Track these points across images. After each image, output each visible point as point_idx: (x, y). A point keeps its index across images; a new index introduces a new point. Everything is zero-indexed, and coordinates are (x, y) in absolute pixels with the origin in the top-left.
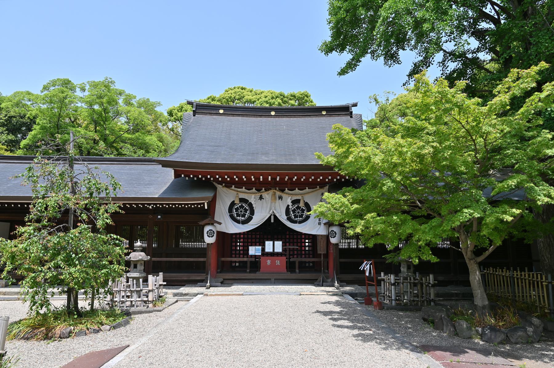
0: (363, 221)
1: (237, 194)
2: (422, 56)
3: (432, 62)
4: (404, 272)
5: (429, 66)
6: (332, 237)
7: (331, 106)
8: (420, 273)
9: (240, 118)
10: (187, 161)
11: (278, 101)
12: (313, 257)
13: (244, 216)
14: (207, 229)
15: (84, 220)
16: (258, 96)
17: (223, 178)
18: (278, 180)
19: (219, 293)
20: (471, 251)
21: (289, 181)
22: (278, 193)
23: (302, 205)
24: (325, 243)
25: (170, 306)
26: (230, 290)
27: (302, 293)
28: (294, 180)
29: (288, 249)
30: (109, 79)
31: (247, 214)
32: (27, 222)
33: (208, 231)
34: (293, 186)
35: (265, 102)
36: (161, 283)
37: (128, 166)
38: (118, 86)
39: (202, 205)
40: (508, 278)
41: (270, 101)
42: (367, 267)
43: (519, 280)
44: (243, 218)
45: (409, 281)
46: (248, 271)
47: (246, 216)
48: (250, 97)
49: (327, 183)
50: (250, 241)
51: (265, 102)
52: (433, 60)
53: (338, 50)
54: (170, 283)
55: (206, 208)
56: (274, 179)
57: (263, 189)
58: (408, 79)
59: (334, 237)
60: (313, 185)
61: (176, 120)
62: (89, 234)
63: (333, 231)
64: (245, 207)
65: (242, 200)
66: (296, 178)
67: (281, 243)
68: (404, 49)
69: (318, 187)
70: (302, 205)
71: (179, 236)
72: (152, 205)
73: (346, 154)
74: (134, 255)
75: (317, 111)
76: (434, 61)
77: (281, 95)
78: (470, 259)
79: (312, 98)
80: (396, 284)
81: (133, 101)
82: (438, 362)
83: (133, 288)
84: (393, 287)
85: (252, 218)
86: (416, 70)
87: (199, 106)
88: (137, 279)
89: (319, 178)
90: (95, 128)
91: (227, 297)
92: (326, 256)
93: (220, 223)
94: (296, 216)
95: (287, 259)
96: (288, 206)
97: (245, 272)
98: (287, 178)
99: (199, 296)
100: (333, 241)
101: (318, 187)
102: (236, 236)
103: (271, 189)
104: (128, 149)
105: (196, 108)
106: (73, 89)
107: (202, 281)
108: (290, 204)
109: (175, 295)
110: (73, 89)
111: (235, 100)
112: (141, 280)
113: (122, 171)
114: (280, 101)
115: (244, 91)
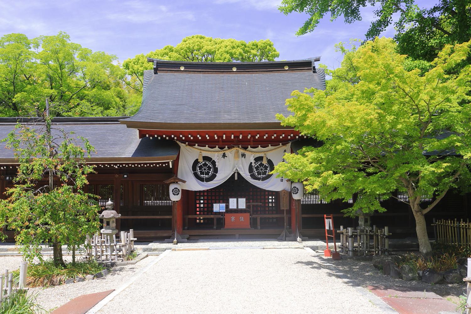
0: (321, 178)
1: (201, 152)
2: (380, 16)
3: (390, 22)
4: (361, 225)
5: (387, 25)
6: (294, 194)
7: (294, 61)
8: (377, 227)
9: (201, 75)
10: (151, 121)
11: (239, 50)
12: (277, 214)
13: (207, 173)
14: (172, 187)
15: (65, 181)
16: (218, 46)
17: (187, 137)
18: (241, 138)
19: (186, 248)
20: (418, 204)
21: (252, 139)
22: (241, 151)
23: (265, 162)
24: (288, 198)
25: (142, 259)
26: (196, 245)
27: (265, 247)
28: (257, 138)
29: (252, 206)
30: (63, 33)
31: (211, 172)
32: (15, 184)
33: (173, 190)
34: (255, 143)
35: (225, 52)
36: (132, 239)
37: (92, 126)
38: (73, 41)
39: (167, 164)
40: (456, 228)
41: (231, 51)
42: (328, 223)
43: (464, 229)
44: (207, 176)
45: (365, 233)
46: (215, 227)
47: (210, 174)
48: (209, 48)
49: (290, 140)
50: (214, 198)
51: (225, 52)
52: (391, 20)
53: (297, 10)
54: (141, 240)
55: (171, 167)
56: (237, 137)
57: (226, 147)
58: (366, 39)
59: (296, 194)
60: (276, 143)
61: (132, 73)
62: (71, 194)
63: (296, 187)
64: (209, 165)
65: (206, 158)
66: (258, 136)
67: (244, 200)
68: (364, 6)
69: (281, 144)
70: (265, 162)
71: (143, 196)
72: (118, 165)
73: (305, 117)
74: (106, 213)
75: (279, 66)
76: (392, 20)
77: (243, 45)
78: (417, 212)
79: (274, 47)
80: (353, 236)
81: (90, 56)
82: (379, 298)
83: (108, 243)
84: (350, 239)
85: (216, 176)
86: (374, 31)
87: (160, 63)
88: (111, 235)
89: (282, 136)
90: (51, 85)
91: (194, 251)
92: (289, 211)
93: (184, 182)
94: (259, 173)
95: (250, 215)
96: (251, 163)
97: (212, 228)
98: (250, 136)
99: (167, 251)
100: (296, 197)
101: (281, 144)
102: (200, 194)
103: (234, 147)
104: (87, 106)
105: (157, 65)
106: (28, 45)
107: (169, 237)
108: (253, 161)
109: (145, 250)
110: (28, 45)
111: (194, 51)
112: (114, 236)
113: (87, 132)
114: (242, 51)
115: (202, 40)
